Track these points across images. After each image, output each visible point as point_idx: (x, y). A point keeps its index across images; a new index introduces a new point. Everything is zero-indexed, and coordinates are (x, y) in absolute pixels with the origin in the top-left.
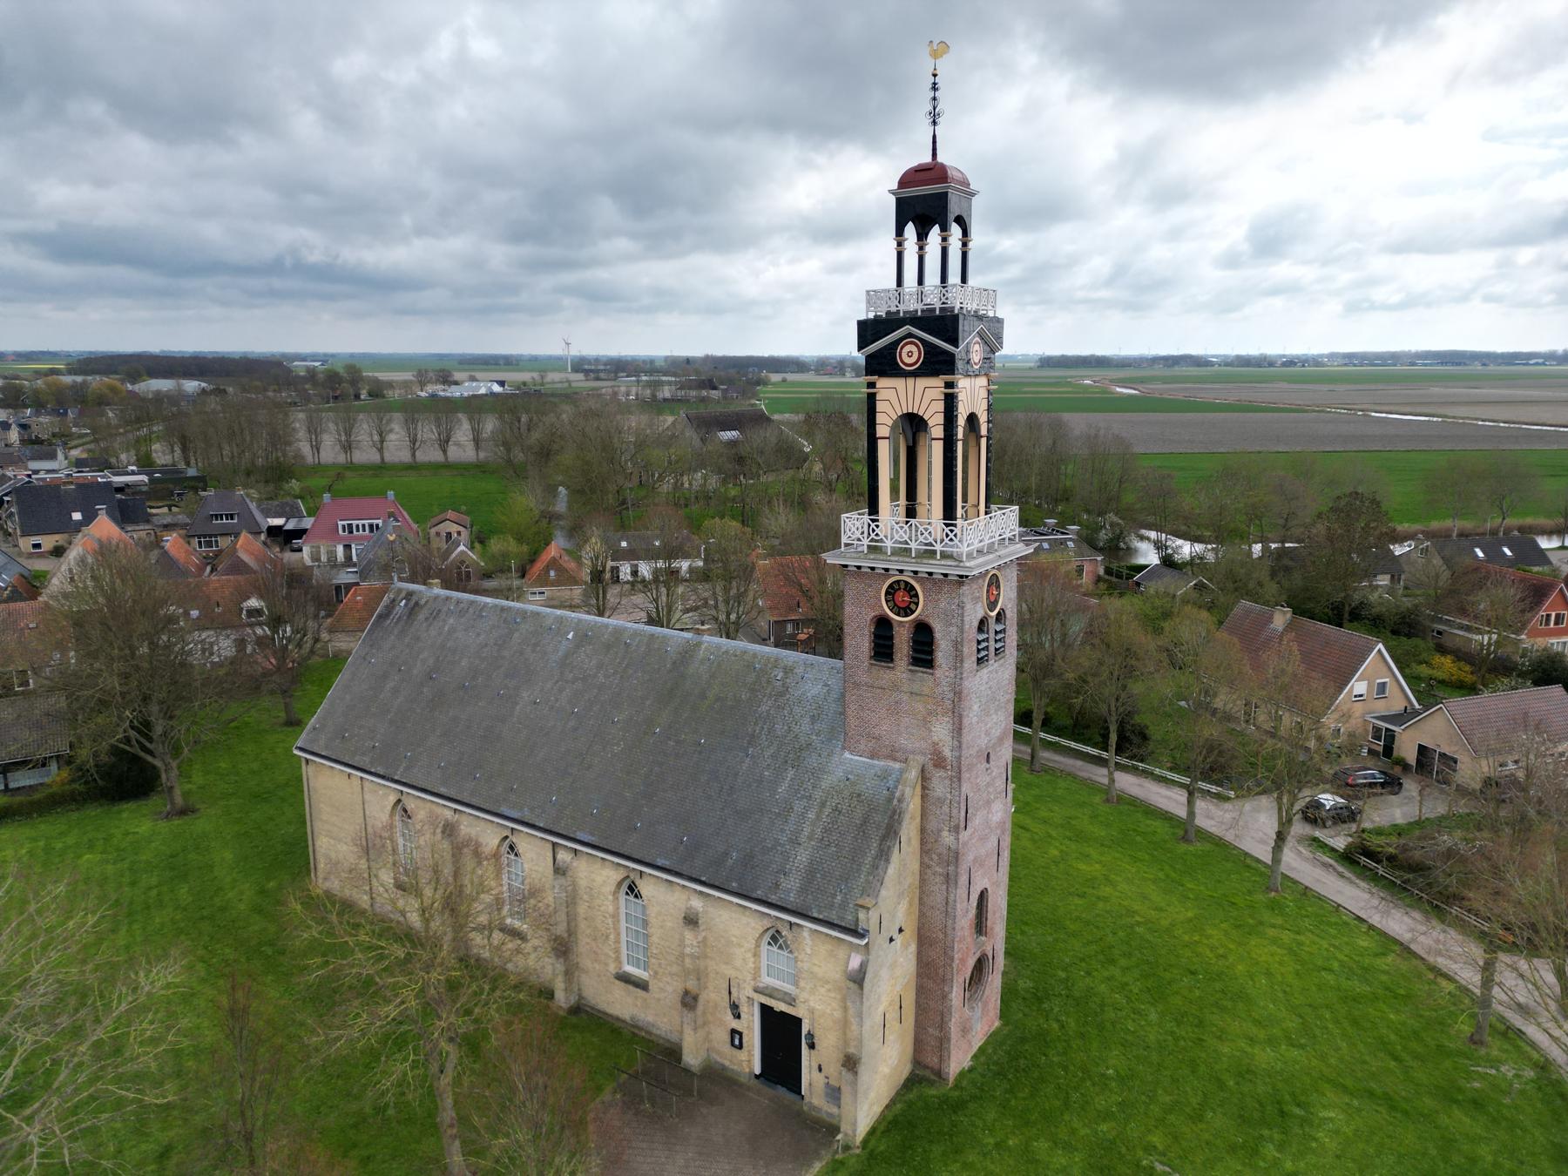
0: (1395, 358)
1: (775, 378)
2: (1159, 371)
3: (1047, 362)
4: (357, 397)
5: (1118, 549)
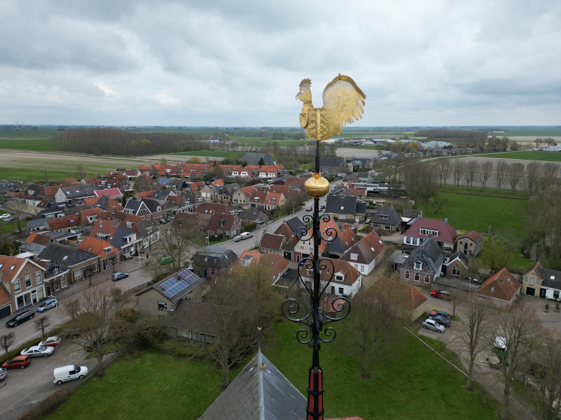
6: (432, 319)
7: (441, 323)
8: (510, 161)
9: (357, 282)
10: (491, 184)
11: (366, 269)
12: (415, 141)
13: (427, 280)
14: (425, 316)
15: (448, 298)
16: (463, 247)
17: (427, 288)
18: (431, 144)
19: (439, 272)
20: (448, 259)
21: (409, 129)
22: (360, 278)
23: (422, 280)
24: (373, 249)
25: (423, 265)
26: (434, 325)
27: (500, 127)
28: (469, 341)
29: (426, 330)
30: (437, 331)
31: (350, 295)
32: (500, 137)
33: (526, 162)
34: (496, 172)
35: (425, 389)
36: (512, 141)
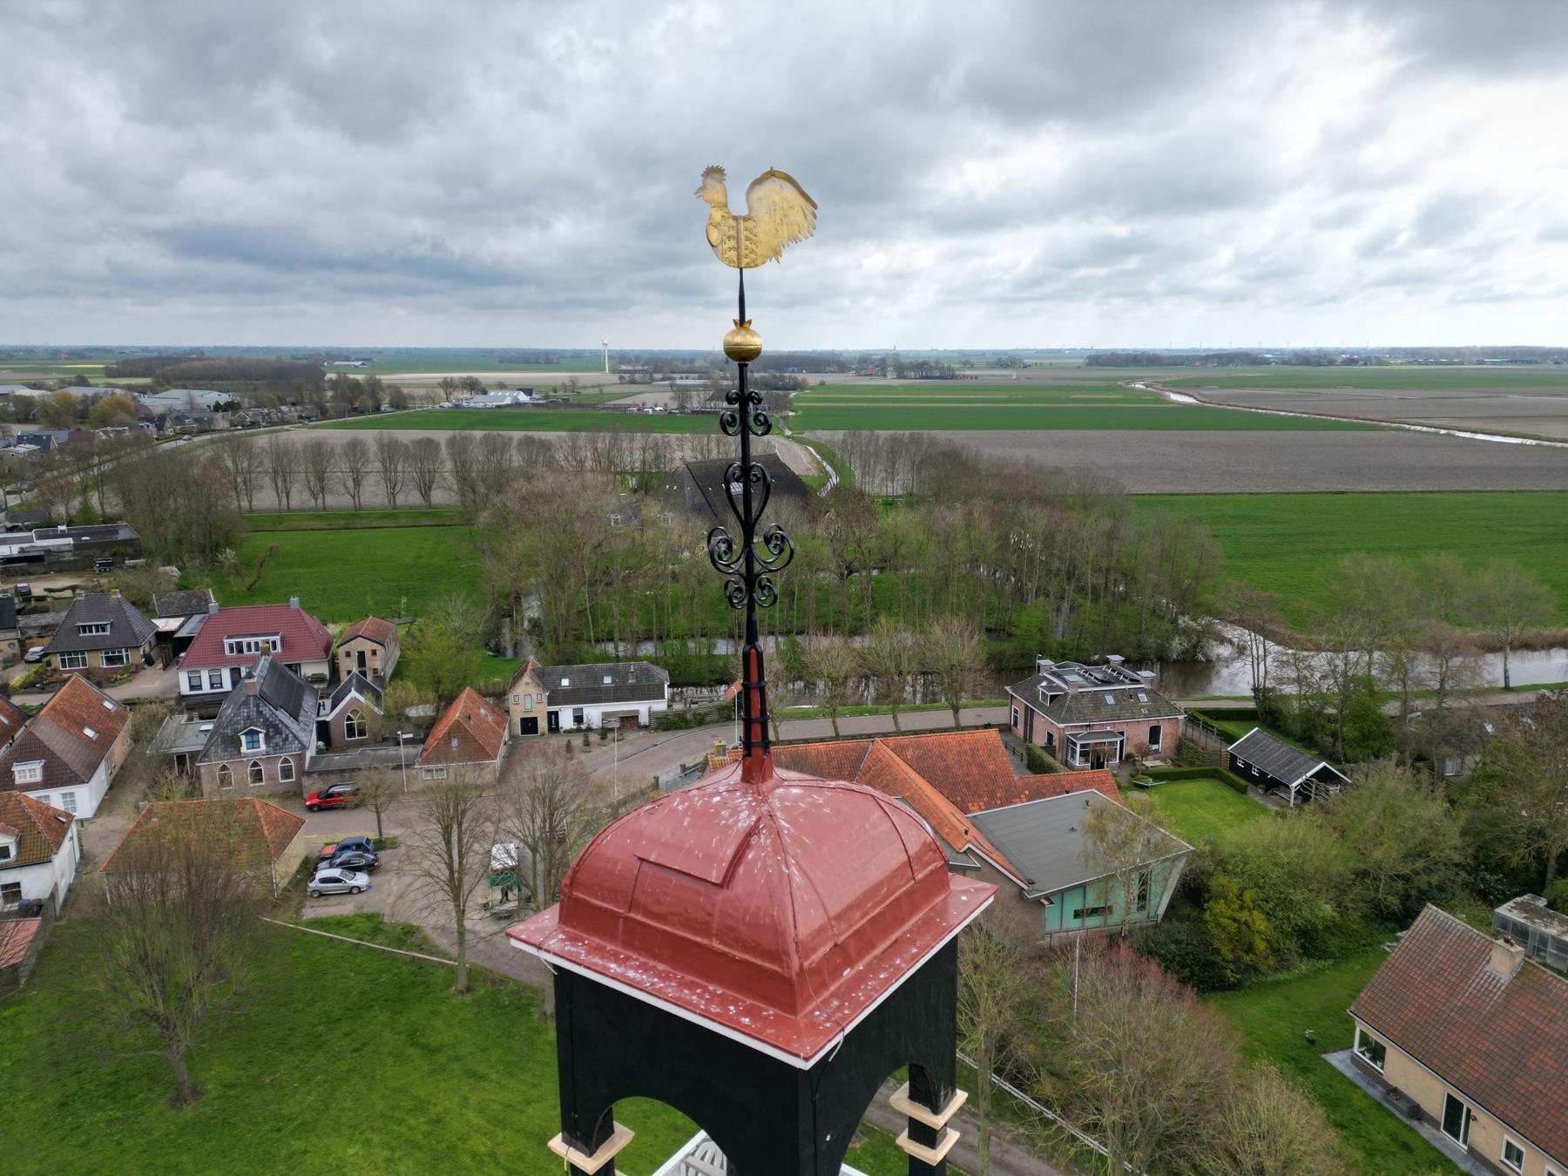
0: (1458, 355)
1: (813, 379)
2: (1214, 371)
3: (1100, 360)
4: (377, 409)
5: (1195, 661)
6: (331, 866)
7: (355, 869)
8: (406, 436)
9: (67, 846)
10: (373, 494)
11: (84, 799)
12: (118, 391)
13: (287, 773)
14: (309, 867)
15: (355, 802)
16: (356, 663)
17: (294, 794)
18: (174, 399)
19: (313, 744)
20: (328, 702)
21: (79, 354)
22: (73, 830)
23: (272, 778)
24: (89, 732)
25: (267, 736)
26: (339, 881)
27: (348, 350)
28: (444, 874)
29: (322, 902)
30: (350, 893)
31: (53, 896)
32: (360, 377)
33: (442, 436)
34: (378, 465)
35: (365, 1044)
36: (389, 386)
